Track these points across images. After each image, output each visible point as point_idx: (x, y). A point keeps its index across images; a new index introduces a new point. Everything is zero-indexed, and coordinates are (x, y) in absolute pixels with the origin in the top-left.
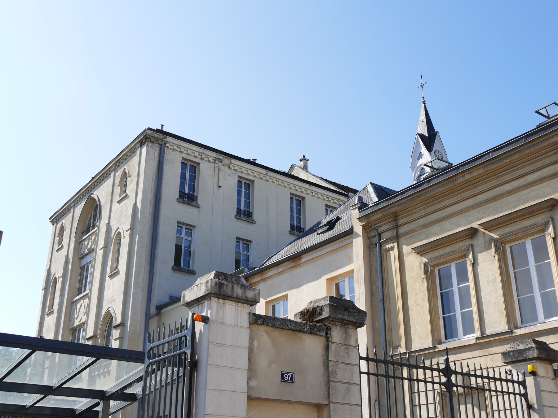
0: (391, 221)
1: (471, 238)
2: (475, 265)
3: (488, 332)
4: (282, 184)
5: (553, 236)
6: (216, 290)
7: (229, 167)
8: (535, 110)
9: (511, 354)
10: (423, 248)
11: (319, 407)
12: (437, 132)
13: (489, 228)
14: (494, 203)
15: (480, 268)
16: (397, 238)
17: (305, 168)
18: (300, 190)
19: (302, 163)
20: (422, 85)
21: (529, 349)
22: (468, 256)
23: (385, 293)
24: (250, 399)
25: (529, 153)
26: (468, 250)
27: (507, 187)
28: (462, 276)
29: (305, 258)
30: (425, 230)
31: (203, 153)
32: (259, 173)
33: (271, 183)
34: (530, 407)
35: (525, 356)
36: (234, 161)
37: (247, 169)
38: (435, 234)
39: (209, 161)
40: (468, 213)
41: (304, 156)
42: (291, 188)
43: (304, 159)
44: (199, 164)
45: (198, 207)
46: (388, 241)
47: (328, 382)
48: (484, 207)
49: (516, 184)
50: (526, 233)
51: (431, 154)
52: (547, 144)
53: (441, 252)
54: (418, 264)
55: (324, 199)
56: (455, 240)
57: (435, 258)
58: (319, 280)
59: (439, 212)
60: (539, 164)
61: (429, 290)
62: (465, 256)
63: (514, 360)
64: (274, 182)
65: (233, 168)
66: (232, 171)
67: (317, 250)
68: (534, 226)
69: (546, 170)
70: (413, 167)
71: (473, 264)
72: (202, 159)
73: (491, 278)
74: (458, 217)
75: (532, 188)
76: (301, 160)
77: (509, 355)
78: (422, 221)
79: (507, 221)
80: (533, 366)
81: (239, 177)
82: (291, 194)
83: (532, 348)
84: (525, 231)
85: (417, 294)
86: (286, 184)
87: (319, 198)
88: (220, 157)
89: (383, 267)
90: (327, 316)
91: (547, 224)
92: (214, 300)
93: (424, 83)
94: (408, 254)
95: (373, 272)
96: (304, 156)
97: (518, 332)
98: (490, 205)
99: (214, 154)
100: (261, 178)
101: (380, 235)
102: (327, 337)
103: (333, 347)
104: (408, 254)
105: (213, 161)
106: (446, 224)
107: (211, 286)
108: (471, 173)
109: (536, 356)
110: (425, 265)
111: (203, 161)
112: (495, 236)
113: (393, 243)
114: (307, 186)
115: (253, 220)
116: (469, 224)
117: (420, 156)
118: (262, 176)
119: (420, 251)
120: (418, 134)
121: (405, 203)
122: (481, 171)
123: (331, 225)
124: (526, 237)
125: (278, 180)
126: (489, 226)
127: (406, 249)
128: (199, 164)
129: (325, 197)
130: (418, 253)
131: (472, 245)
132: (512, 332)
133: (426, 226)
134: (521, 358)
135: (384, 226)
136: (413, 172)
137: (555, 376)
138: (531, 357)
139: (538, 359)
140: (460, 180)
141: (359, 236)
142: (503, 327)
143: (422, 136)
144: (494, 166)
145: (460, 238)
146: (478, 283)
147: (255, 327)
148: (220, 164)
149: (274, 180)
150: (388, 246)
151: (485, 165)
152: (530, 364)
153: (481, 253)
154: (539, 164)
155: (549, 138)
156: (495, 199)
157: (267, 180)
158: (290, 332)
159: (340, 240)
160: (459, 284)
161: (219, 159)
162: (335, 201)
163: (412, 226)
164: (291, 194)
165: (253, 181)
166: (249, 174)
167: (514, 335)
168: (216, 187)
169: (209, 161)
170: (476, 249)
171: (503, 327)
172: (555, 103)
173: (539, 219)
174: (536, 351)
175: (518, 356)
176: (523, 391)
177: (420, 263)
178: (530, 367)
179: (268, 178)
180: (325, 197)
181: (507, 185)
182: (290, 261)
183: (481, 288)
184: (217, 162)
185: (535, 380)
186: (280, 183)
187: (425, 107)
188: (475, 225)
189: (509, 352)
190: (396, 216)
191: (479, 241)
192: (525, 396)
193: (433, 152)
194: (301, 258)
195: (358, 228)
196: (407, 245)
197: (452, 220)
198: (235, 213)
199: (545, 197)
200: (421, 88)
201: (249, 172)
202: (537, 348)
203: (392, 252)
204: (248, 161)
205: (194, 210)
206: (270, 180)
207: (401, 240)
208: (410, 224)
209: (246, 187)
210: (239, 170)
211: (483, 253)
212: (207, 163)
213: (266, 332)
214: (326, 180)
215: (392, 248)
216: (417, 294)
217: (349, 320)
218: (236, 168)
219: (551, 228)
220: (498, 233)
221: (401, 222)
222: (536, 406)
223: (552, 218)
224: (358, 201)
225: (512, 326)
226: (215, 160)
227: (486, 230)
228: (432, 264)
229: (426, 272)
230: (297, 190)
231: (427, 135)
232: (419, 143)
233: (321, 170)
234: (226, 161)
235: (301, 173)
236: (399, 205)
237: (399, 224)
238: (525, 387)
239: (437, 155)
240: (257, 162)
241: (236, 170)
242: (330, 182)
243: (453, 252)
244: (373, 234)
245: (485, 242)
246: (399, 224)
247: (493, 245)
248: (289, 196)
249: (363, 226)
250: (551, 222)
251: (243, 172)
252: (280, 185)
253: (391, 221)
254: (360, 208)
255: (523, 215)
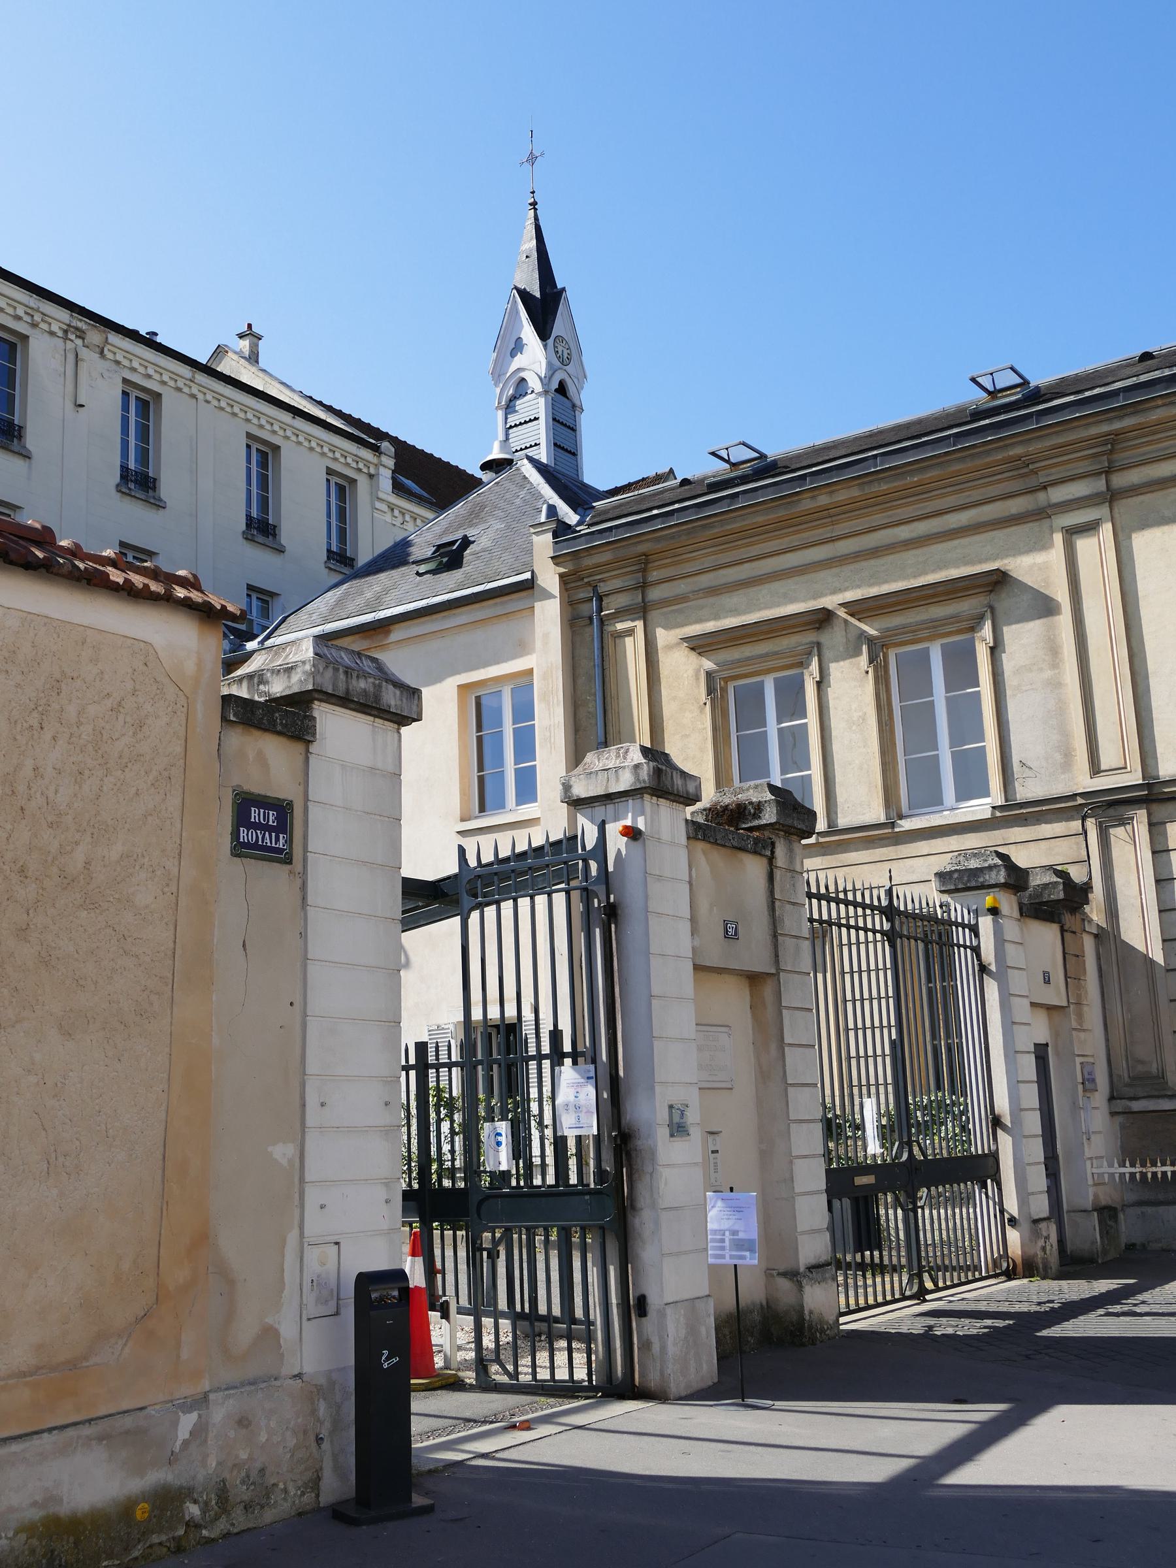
0: (632, 572)
1: (818, 629)
2: (823, 686)
3: (843, 822)
4: (228, 409)
5: (991, 644)
6: (654, 784)
7: (102, 353)
8: (970, 376)
9: (956, 876)
10: (709, 640)
11: (754, 979)
12: (564, 289)
13: (859, 612)
14: (872, 562)
15: (834, 693)
16: (642, 611)
17: (253, 358)
18: (255, 421)
19: (245, 345)
20: (532, 159)
21: (990, 868)
22: (809, 665)
23: (610, 728)
24: (697, 968)
25: (959, 471)
26: (810, 654)
27: (904, 532)
28: (792, 704)
29: (397, 633)
30: (711, 600)
31: (38, 310)
32: (175, 376)
33: (201, 403)
34: (983, 969)
35: (981, 880)
36: (114, 338)
37: (145, 363)
38: (735, 612)
39: (52, 333)
40: (813, 575)
41: (250, 326)
42: (248, 420)
43: (249, 333)
44: (25, 338)
45: (27, 456)
46: (621, 614)
47: (775, 936)
48: (852, 567)
49: (922, 528)
50: (934, 630)
51: (545, 347)
52: (1000, 457)
53: (748, 651)
54: (691, 672)
55: (323, 454)
56: (784, 629)
57: (733, 662)
58: (438, 686)
59: (746, 565)
60: (976, 495)
61: (715, 729)
62: (803, 664)
63: (960, 886)
64: (208, 402)
65: (110, 356)
66: (107, 364)
67: (434, 616)
68: (955, 618)
69: (986, 509)
70: (497, 374)
71: (819, 683)
72: (34, 325)
73: (856, 715)
74: (790, 581)
75: (956, 542)
76: (241, 336)
77: (951, 878)
78: (705, 580)
79: (899, 603)
80: (995, 899)
81: (125, 381)
82: (249, 435)
83: (996, 866)
84: (934, 627)
85: (687, 736)
86: (236, 410)
87: (311, 449)
88: (80, 325)
89: (607, 672)
90: (773, 820)
91: (981, 618)
92: (647, 797)
93: (536, 153)
94: (669, 647)
95: (581, 681)
96: (250, 326)
97: (906, 825)
98: (864, 564)
99: (64, 315)
100: (179, 390)
101: (600, 599)
102: (771, 859)
103: (778, 874)
104: (669, 647)
105: (60, 334)
106: (763, 592)
107: (649, 775)
108: (833, 492)
109: (1003, 881)
110: (709, 675)
111: (37, 331)
112: (872, 632)
113: (633, 620)
114: (286, 417)
115: (160, 500)
116: (815, 598)
117: (518, 347)
118: (180, 384)
119: (699, 645)
120: (516, 288)
121: (672, 537)
122: (855, 492)
123: (450, 557)
124: (931, 638)
125: (219, 396)
126: (858, 609)
127: (663, 636)
128: (25, 338)
129: (326, 450)
130: (693, 649)
131: (819, 645)
132: (893, 825)
133: (714, 591)
134: (973, 884)
135: (614, 581)
136: (496, 385)
137: (1021, 915)
138: (992, 882)
139: (1005, 886)
140: (807, 504)
141: (551, 596)
142: (875, 813)
143: (524, 295)
144: (884, 487)
145: (794, 626)
146: (826, 723)
147: (692, 842)
148: (79, 342)
149: (209, 397)
150: (620, 626)
151: (866, 480)
152: (988, 894)
153: (837, 661)
154: (976, 495)
155: (1006, 446)
156: (875, 552)
157: (193, 396)
158: (729, 851)
159: (498, 600)
160: (779, 721)
161: (77, 329)
162: (349, 460)
163: (681, 587)
164: (249, 435)
165: (159, 395)
166: (149, 376)
167: (897, 830)
168: (69, 405)
169: (52, 333)
170: (827, 654)
171: (875, 813)
172: (1012, 369)
173: (966, 606)
174: (1003, 873)
175: (969, 881)
176: (975, 943)
177: (697, 672)
178: (989, 901)
179: (195, 390)
180: (326, 450)
181: (902, 528)
182: (357, 636)
183: (834, 734)
184: (73, 337)
185: (995, 922)
186: (223, 404)
187: (536, 218)
188: (830, 602)
189: (952, 872)
190: (644, 562)
191: (833, 638)
192: (976, 950)
193: (550, 341)
194: (388, 632)
195: (549, 578)
196: (666, 627)
197: (777, 586)
198: (118, 480)
199: (980, 562)
200: (527, 166)
201: (151, 371)
202: (1005, 866)
203: (629, 641)
204: (133, 335)
205: (18, 463)
206: (200, 396)
207: (654, 615)
208: (675, 583)
209: (142, 407)
210: (126, 363)
211: (842, 663)
212: (46, 336)
213: (704, 852)
214: (320, 403)
215: (630, 632)
216: (687, 736)
217: (786, 823)
218: (119, 357)
219: (988, 626)
220: (877, 625)
221: (654, 575)
222: (993, 968)
223: (992, 609)
224: (548, 516)
225: (894, 814)
226: (66, 332)
227: (852, 615)
228: (725, 674)
229: (710, 691)
230: (261, 427)
231: (538, 295)
232: (517, 312)
233: (297, 368)
234: (95, 336)
235: (243, 371)
236: (658, 540)
237: (650, 579)
238: (977, 935)
239: (560, 349)
240: (159, 339)
241: (118, 363)
242: (329, 409)
243: (776, 653)
244: (582, 595)
245: (848, 640)
246: (650, 579)
247: (865, 648)
248: (244, 441)
249: (561, 576)
250: (989, 614)
251: (134, 370)
252: (222, 409)
253: (632, 572)
254: (555, 535)
255: (934, 596)
